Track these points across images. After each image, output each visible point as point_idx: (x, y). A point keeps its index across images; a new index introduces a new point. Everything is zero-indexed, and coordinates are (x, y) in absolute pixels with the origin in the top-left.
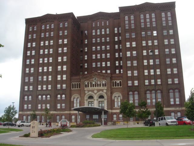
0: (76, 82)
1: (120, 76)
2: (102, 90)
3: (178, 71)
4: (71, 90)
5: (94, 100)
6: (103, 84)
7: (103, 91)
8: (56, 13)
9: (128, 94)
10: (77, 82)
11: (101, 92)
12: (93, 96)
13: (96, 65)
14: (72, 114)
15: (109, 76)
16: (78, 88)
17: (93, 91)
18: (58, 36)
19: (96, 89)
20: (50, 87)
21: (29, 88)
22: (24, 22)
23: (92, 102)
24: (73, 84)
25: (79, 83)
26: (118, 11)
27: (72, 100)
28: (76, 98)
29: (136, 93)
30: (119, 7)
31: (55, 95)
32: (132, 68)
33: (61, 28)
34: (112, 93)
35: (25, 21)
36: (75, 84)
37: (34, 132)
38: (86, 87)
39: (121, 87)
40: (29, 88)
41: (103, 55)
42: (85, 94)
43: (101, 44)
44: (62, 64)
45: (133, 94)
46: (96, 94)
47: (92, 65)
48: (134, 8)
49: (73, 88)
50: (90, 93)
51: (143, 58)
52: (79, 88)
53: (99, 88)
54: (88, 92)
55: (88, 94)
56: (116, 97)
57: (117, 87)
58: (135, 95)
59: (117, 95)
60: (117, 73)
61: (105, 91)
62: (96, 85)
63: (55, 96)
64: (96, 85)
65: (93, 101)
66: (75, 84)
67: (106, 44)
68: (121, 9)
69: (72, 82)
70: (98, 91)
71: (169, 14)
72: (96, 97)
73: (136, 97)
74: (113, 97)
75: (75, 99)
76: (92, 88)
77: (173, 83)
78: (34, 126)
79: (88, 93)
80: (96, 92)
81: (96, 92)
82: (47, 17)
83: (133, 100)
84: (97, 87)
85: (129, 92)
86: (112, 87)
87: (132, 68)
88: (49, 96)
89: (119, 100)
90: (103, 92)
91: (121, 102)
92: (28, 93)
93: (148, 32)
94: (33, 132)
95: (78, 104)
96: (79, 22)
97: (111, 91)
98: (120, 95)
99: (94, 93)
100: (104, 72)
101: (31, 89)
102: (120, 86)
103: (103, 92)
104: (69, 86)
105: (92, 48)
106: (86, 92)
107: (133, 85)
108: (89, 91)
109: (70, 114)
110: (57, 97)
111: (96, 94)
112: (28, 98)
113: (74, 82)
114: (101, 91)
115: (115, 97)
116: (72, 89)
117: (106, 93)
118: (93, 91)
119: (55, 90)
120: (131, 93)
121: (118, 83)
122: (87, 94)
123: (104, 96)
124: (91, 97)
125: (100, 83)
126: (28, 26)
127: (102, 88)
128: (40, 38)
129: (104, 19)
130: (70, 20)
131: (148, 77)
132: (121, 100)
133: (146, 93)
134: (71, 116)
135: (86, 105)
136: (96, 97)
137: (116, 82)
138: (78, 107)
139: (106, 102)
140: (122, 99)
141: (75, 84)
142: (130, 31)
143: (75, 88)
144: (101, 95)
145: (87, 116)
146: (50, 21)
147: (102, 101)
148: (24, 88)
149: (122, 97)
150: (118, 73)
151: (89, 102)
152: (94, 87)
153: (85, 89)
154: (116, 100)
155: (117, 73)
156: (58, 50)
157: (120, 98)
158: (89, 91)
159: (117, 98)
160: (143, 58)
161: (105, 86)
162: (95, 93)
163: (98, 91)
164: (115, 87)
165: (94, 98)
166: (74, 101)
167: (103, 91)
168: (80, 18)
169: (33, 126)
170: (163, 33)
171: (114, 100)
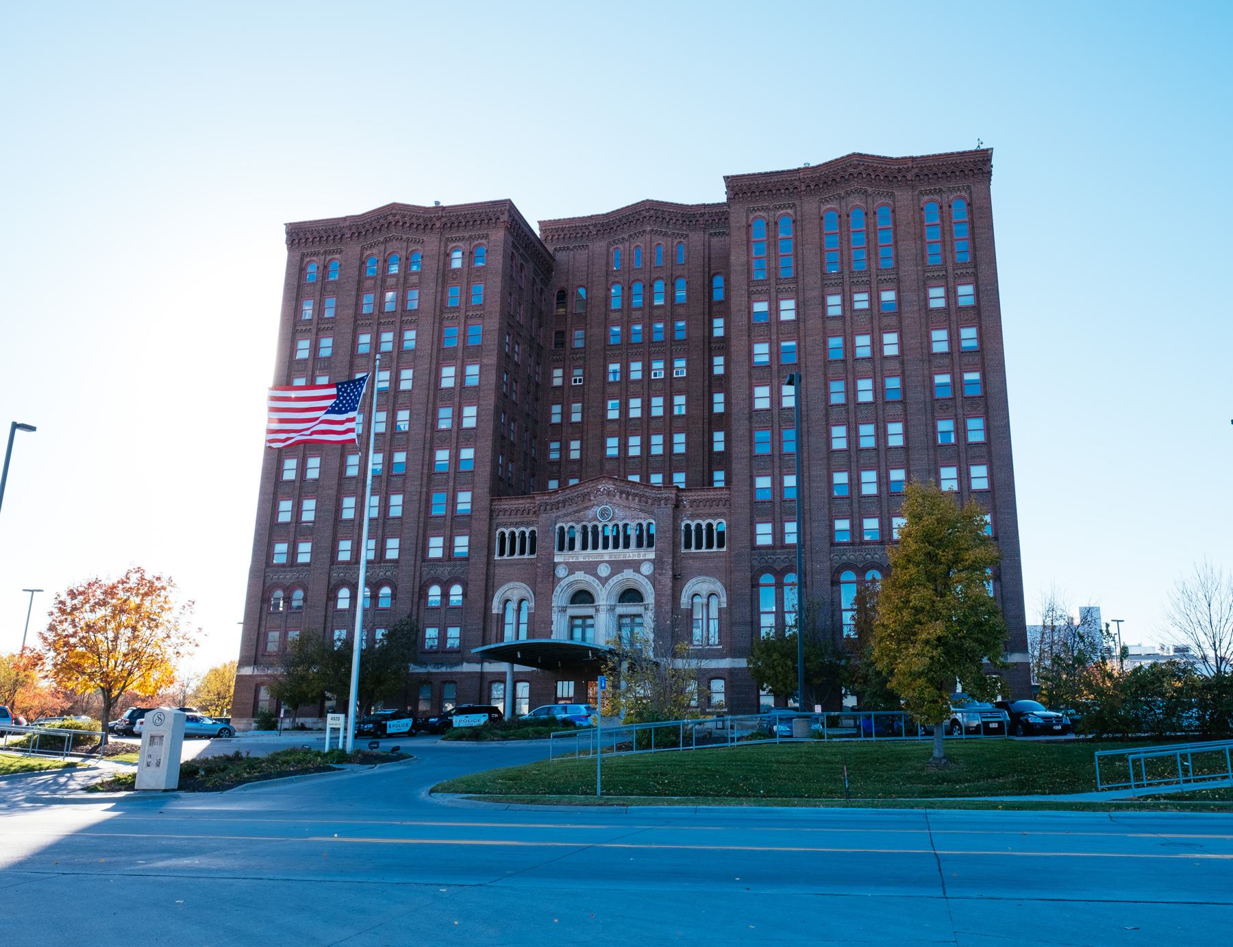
0: (517, 525)
1: (720, 500)
2: (635, 565)
3: (991, 477)
4: (489, 562)
5: (612, 609)
6: (606, 539)
7: (637, 570)
8: (437, 203)
9: (755, 585)
10: (511, 524)
11: (628, 573)
12: (591, 590)
13: (624, 446)
14: (490, 678)
15: (667, 499)
16: (526, 556)
17: (591, 568)
18: (442, 312)
19: (606, 558)
20: (305, 552)
21: (293, 553)
22: (284, 236)
23: (589, 622)
24: (503, 534)
25: (531, 529)
26: (718, 195)
27: (495, 611)
28: (516, 598)
29: (791, 578)
30: (726, 178)
31: (417, 584)
32: (777, 464)
33: (455, 271)
34: (678, 579)
35: (287, 233)
36: (513, 534)
37: (158, 765)
38: (561, 548)
39: (724, 549)
40: (293, 553)
41: (657, 402)
42: (554, 580)
43: (647, 351)
44: (454, 440)
45: (779, 586)
46: (604, 581)
47: (603, 447)
48: (796, 183)
49: (502, 553)
50: (580, 575)
51: (827, 415)
52: (532, 552)
53: (621, 554)
54: (571, 572)
55: (568, 582)
56: (697, 600)
57: (704, 550)
58: (786, 589)
59: (515, 596)
60: (716, 485)
61: (647, 569)
62: (616, 539)
63: (417, 590)
64: (616, 539)
65: (591, 617)
66: (513, 534)
67: (669, 348)
68: (736, 184)
69: (498, 526)
70: (617, 567)
71: (959, 212)
72: (604, 597)
73: (791, 598)
74: (684, 601)
75: (512, 606)
76: (590, 555)
77: (857, 540)
78: (160, 733)
79: (571, 578)
80: (604, 571)
81: (604, 571)
82: (390, 218)
83: (776, 613)
84: (610, 550)
85: (760, 575)
86: (683, 550)
87: (777, 464)
88: (386, 591)
89: (714, 613)
90: (639, 572)
91: (720, 619)
92: (445, 572)
93: (857, 297)
94: (154, 762)
95: (523, 629)
96: (550, 249)
97: (673, 569)
98: (718, 587)
99: (596, 575)
100: (656, 479)
101: (304, 558)
102: (721, 545)
103: (639, 572)
104: (485, 547)
105: (605, 368)
106: (561, 572)
107: (857, 540)
108: (572, 568)
109: (482, 675)
110: (423, 595)
111: (604, 581)
112: (445, 595)
113: (505, 525)
114: (629, 568)
115: (711, 595)
116: (497, 557)
117: (653, 579)
118: (591, 568)
119: (418, 563)
120: (767, 579)
121: (721, 534)
122: (563, 583)
123: (642, 590)
124: (583, 596)
125: (615, 533)
126: (302, 260)
127: (632, 554)
128: (356, 320)
129: (665, 234)
130: (498, 236)
131: (851, 504)
132: (720, 610)
133: (836, 583)
134: (486, 684)
135: (559, 633)
136: (604, 597)
137: (710, 526)
138: (523, 637)
139: (649, 619)
140: (724, 605)
141: (513, 534)
142: (773, 290)
143: (699, 546)
144: (631, 585)
145: (560, 684)
146: (404, 237)
147: (585, 618)
148: (270, 554)
149: (724, 599)
150: (722, 484)
151: (573, 618)
152: (600, 550)
153: (556, 560)
154: (698, 615)
155: (716, 485)
156: (438, 378)
157: (719, 603)
158: (572, 568)
159: (705, 601)
160: (827, 415)
161: (650, 545)
162: (599, 578)
163: (617, 567)
164: (693, 550)
165: (596, 598)
166: (692, 610)
167: (637, 570)
168: (560, 229)
169: (154, 733)
170: (926, 299)
171: (503, 616)
